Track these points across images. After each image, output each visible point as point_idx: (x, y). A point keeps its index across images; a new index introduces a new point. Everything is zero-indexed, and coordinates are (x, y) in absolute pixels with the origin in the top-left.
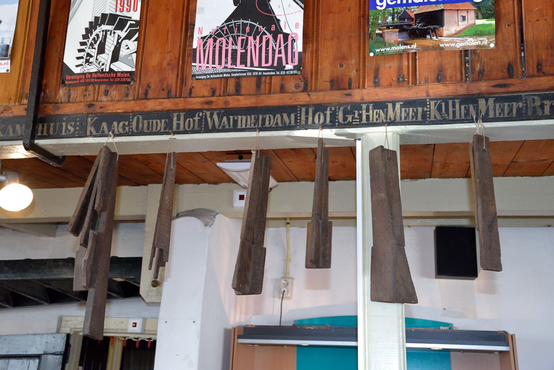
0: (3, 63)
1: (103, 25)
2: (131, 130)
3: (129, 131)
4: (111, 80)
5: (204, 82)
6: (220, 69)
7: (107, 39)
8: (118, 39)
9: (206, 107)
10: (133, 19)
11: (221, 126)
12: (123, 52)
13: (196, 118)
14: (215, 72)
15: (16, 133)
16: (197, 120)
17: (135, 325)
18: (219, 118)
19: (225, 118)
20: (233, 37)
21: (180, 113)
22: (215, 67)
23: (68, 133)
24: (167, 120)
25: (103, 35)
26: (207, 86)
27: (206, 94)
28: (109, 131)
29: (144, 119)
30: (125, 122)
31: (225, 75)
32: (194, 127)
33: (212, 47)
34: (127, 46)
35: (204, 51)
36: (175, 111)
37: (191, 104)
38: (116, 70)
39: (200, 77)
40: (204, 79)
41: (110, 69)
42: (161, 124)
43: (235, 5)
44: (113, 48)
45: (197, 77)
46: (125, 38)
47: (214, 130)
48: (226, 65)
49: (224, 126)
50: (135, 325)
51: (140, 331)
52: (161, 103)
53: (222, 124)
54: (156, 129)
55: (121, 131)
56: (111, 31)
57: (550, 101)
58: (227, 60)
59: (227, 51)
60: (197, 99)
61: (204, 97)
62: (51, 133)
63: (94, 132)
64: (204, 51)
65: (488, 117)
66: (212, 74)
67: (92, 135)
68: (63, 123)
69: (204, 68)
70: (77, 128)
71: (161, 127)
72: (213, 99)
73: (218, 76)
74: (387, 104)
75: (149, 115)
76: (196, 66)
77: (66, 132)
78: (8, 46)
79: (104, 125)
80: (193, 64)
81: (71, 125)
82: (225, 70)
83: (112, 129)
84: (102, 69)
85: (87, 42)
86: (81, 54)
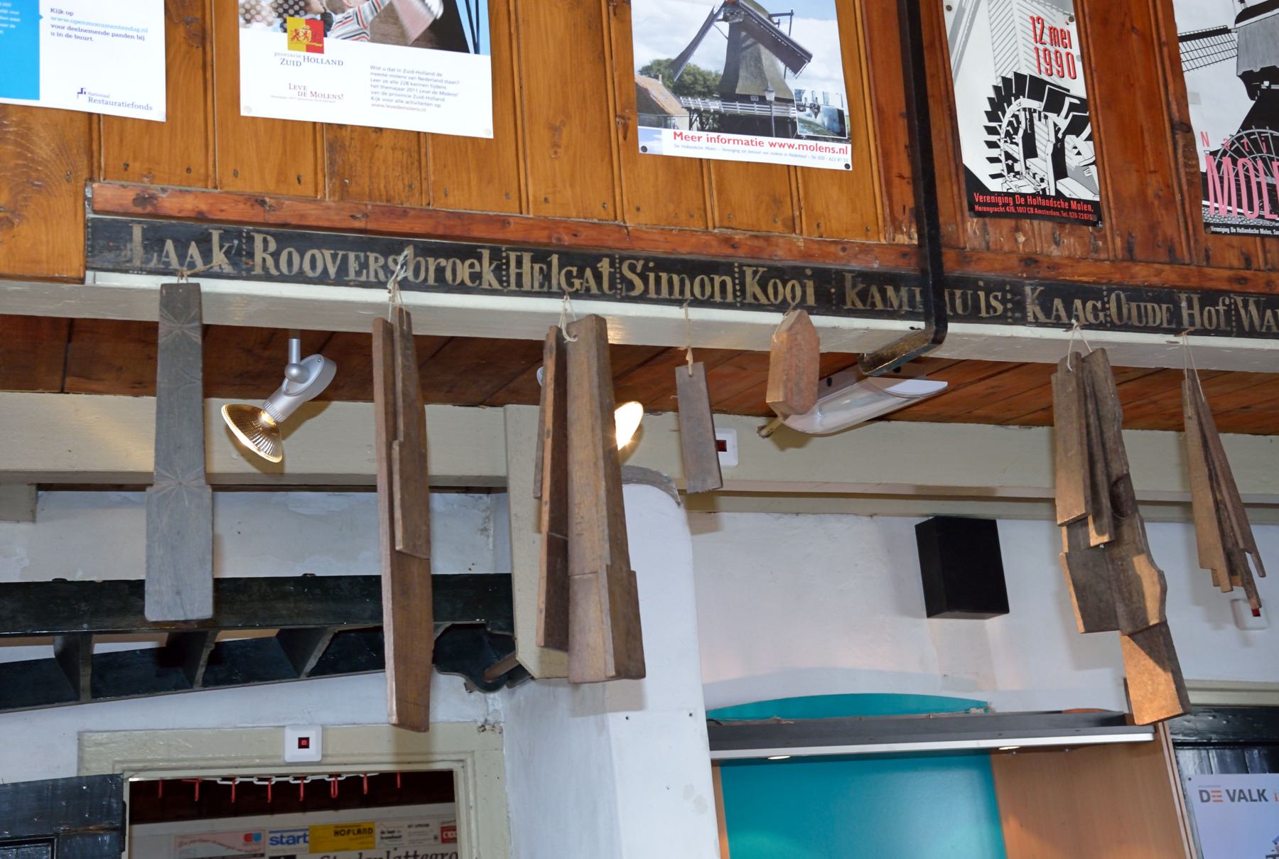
0: (837, 150)
1: (1021, 97)
2: (1109, 319)
3: (1106, 322)
4: (1064, 214)
5: (1226, 238)
6: (1251, 218)
7: (1036, 129)
8: (1057, 132)
9: (1237, 287)
10: (1072, 93)
11: (1264, 328)
12: (1071, 161)
13: (1221, 308)
14: (1244, 222)
15: (889, 303)
16: (1222, 311)
17: (304, 743)
18: (1258, 311)
19: (1269, 313)
20: (1263, 160)
21: (1192, 295)
22: (1242, 214)
23: (992, 311)
24: (1171, 306)
25: (1026, 119)
26: (1233, 247)
27: (1236, 263)
28: (1070, 318)
29: (1129, 299)
30: (1095, 302)
31: (1262, 231)
32: (1218, 324)
33: (1232, 175)
34: (1075, 148)
35: (1221, 179)
36: (1182, 289)
37: (1211, 280)
38: (1068, 196)
39: (1218, 230)
40: (1226, 233)
41: (1057, 191)
42: (1161, 313)
43: (1252, 98)
44: (1050, 149)
45: (1213, 229)
46: (1069, 131)
47: (1252, 333)
48: (1262, 213)
49: (1269, 328)
50: (304, 743)
51: (318, 758)
52: (1158, 273)
53: (1266, 323)
54: (1154, 322)
55: (1091, 318)
56: (1040, 113)
57: (435, 260)
58: (1262, 202)
59: (1259, 184)
60: (1220, 271)
61: (1231, 268)
62: (960, 311)
63: (1042, 318)
64: (1221, 179)
65: (648, 296)
66: (1241, 226)
67: (1038, 324)
68: (979, 292)
69: (1223, 213)
70: (1009, 306)
71: (1162, 319)
72: (1248, 274)
73: (1250, 231)
74: (479, 250)
75: (1137, 294)
76: (1208, 207)
77: (988, 312)
78: (841, 113)
79: (1058, 303)
80: (1204, 202)
81: (996, 298)
82: (1261, 222)
83: (1074, 313)
84: (1044, 190)
85: (998, 128)
86: (994, 153)
